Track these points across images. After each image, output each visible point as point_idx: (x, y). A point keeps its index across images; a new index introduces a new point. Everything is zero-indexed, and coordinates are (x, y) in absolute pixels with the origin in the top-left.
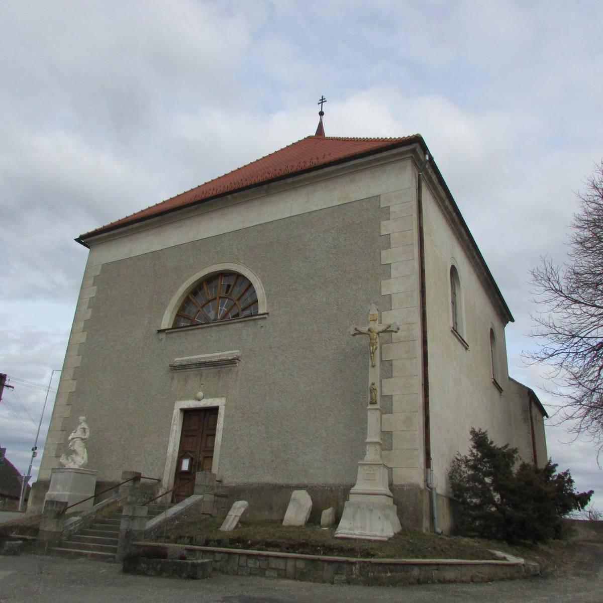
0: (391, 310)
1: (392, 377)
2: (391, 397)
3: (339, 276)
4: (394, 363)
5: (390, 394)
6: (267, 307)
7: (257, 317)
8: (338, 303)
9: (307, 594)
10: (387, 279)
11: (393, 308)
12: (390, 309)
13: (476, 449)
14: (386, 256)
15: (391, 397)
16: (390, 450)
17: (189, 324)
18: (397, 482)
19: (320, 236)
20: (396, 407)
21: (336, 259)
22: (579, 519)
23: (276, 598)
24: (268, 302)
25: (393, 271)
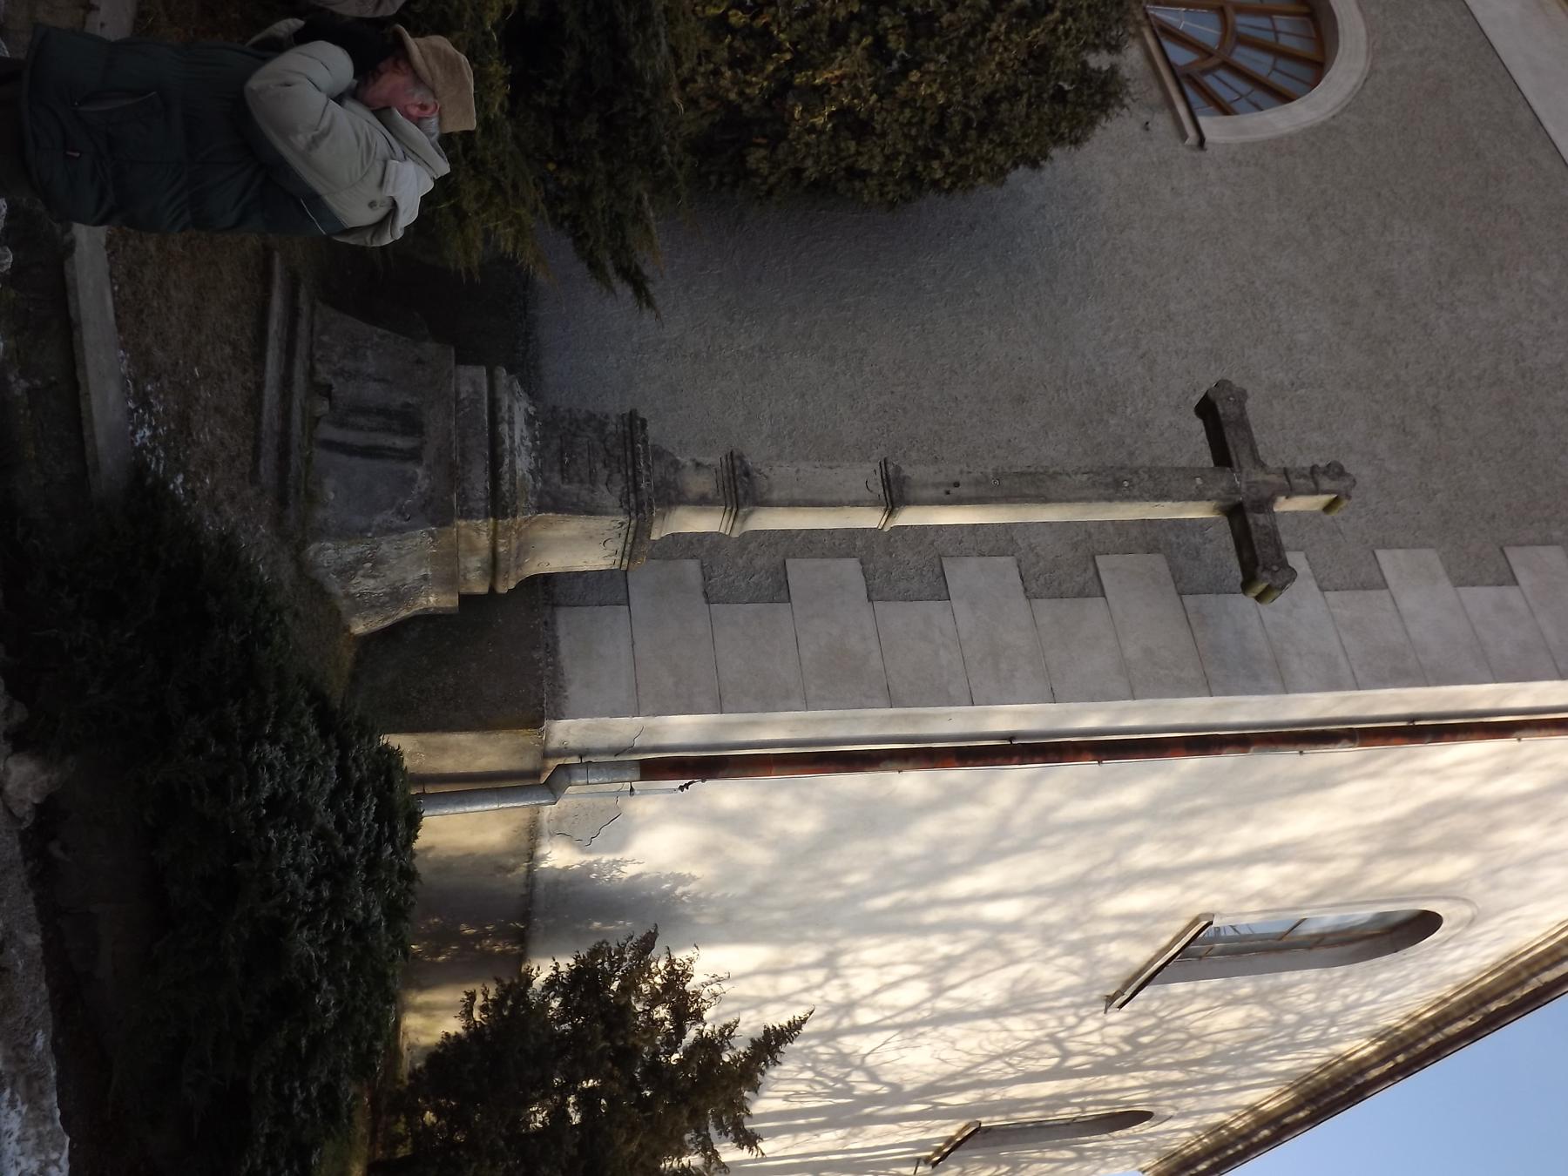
0: (1322, 589)
1: (1029, 595)
2: (941, 592)
3: (1412, 391)
4: (1094, 606)
5: (954, 585)
6: (1227, 145)
7: (1182, 110)
8: (1302, 385)
9: (213, 543)
10: (1448, 572)
11: (1330, 595)
12: (1325, 584)
13: (1105, 67)
14: (746, 1149)
15: (941, 592)
16: (705, 594)
17: (894, 496)
18: (569, 625)
19: (1555, 318)
20: (901, 617)
21: (1479, 379)
22: (1227, 435)
23: (328, 692)
24: (1243, 145)
25: (1492, 592)
